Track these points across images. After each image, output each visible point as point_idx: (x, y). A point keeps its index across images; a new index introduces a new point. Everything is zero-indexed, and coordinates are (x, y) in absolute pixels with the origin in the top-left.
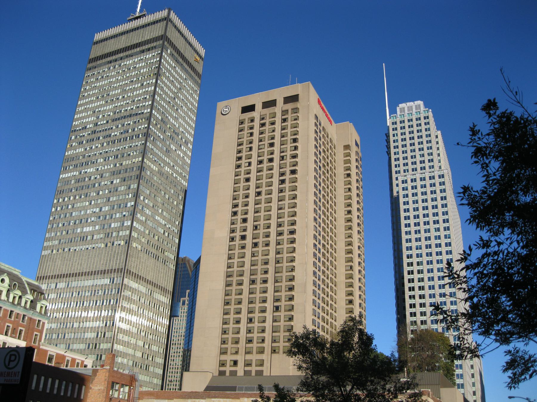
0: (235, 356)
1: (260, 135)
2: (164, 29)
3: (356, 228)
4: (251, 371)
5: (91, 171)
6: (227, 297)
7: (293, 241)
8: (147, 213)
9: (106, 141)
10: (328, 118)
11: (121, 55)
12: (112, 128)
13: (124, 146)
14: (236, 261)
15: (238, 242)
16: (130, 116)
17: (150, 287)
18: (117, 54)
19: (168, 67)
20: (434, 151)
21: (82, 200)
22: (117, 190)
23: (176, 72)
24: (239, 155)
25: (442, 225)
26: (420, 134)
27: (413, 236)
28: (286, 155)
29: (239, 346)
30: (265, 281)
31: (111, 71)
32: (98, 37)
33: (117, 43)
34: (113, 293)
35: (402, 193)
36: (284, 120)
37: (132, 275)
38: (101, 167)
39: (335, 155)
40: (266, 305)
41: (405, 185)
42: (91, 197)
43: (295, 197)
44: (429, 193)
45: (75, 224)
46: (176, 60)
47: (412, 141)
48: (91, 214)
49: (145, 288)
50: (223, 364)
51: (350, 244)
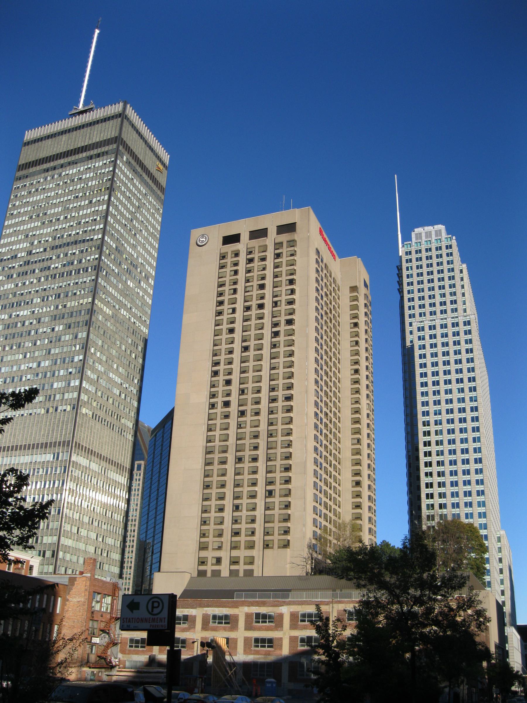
0: (218, 552)
1: (246, 273)
2: (118, 129)
3: (364, 392)
4: (238, 571)
5: (25, 314)
6: (207, 479)
7: (289, 410)
8: (99, 369)
9: (43, 275)
10: (331, 252)
11: (62, 161)
12: (51, 258)
13: (69, 282)
14: (217, 433)
15: (219, 410)
16: (76, 243)
17: (104, 464)
18: (57, 160)
19: (124, 179)
20: (458, 290)
21: (13, 352)
22: (60, 340)
23: (134, 185)
24: (220, 299)
25: (466, 385)
26: (440, 268)
27: (431, 398)
28: (281, 301)
29: (222, 539)
30: (255, 459)
31: (48, 183)
32: (30, 135)
33: (56, 146)
34: (58, 472)
35: (417, 343)
36: (278, 256)
37: (85, 451)
38: (37, 309)
39: (339, 299)
40: (256, 488)
41: (421, 334)
42: (25, 348)
43: (291, 354)
44: (451, 343)
45: (5, 382)
46: (135, 171)
47: (431, 277)
48: (27, 370)
49: (98, 465)
50: (202, 562)
51: (357, 411)
